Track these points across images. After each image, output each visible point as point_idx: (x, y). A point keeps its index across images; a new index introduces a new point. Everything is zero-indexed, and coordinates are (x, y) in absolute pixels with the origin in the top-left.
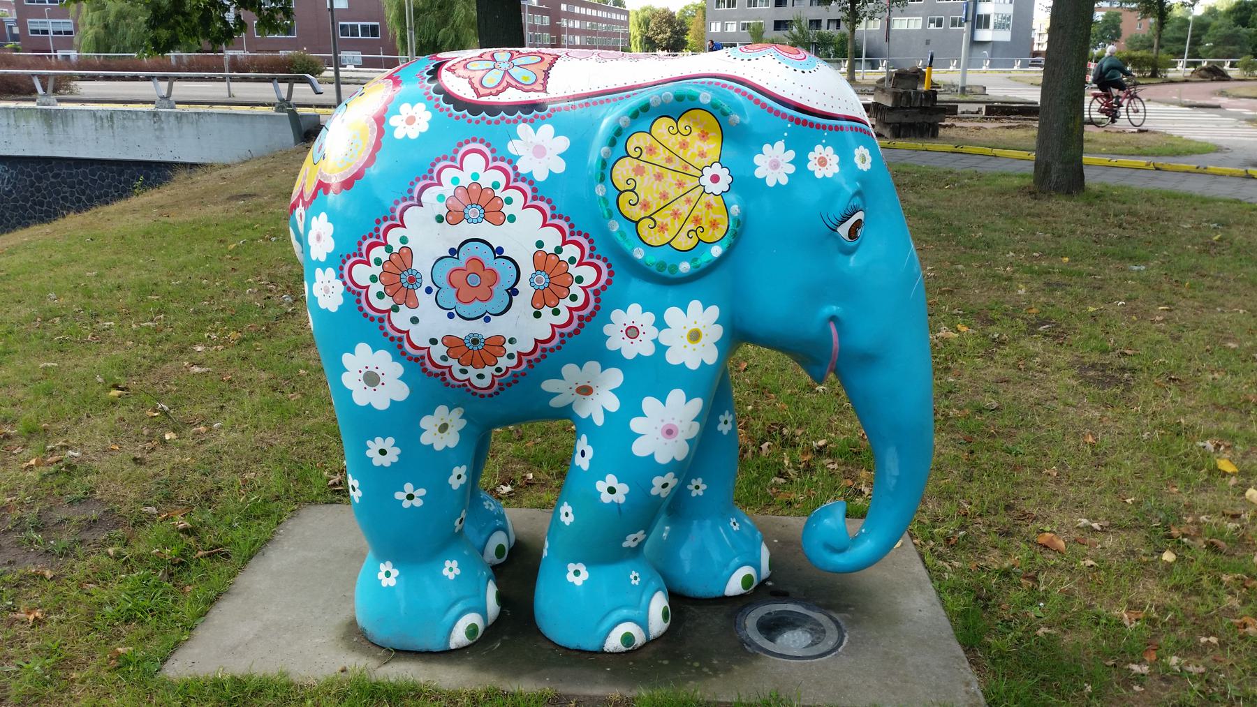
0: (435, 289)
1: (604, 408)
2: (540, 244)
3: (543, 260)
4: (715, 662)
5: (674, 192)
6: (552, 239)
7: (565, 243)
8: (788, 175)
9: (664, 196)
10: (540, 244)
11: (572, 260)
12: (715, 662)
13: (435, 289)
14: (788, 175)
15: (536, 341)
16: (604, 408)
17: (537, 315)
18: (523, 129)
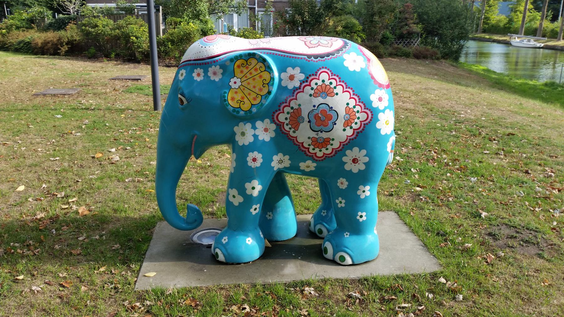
0: (316, 108)
1: (364, 156)
2: (348, 104)
3: (348, 110)
4: (436, 39)
5: (250, 81)
6: (352, 103)
7: (289, 106)
8: (346, 156)
9: (254, 79)
10: (348, 104)
11: (358, 112)
12: (436, 39)
13: (316, 108)
14: (346, 156)
15: (347, 136)
16: (364, 156)
17: (309, 138)
18: (345, 56)
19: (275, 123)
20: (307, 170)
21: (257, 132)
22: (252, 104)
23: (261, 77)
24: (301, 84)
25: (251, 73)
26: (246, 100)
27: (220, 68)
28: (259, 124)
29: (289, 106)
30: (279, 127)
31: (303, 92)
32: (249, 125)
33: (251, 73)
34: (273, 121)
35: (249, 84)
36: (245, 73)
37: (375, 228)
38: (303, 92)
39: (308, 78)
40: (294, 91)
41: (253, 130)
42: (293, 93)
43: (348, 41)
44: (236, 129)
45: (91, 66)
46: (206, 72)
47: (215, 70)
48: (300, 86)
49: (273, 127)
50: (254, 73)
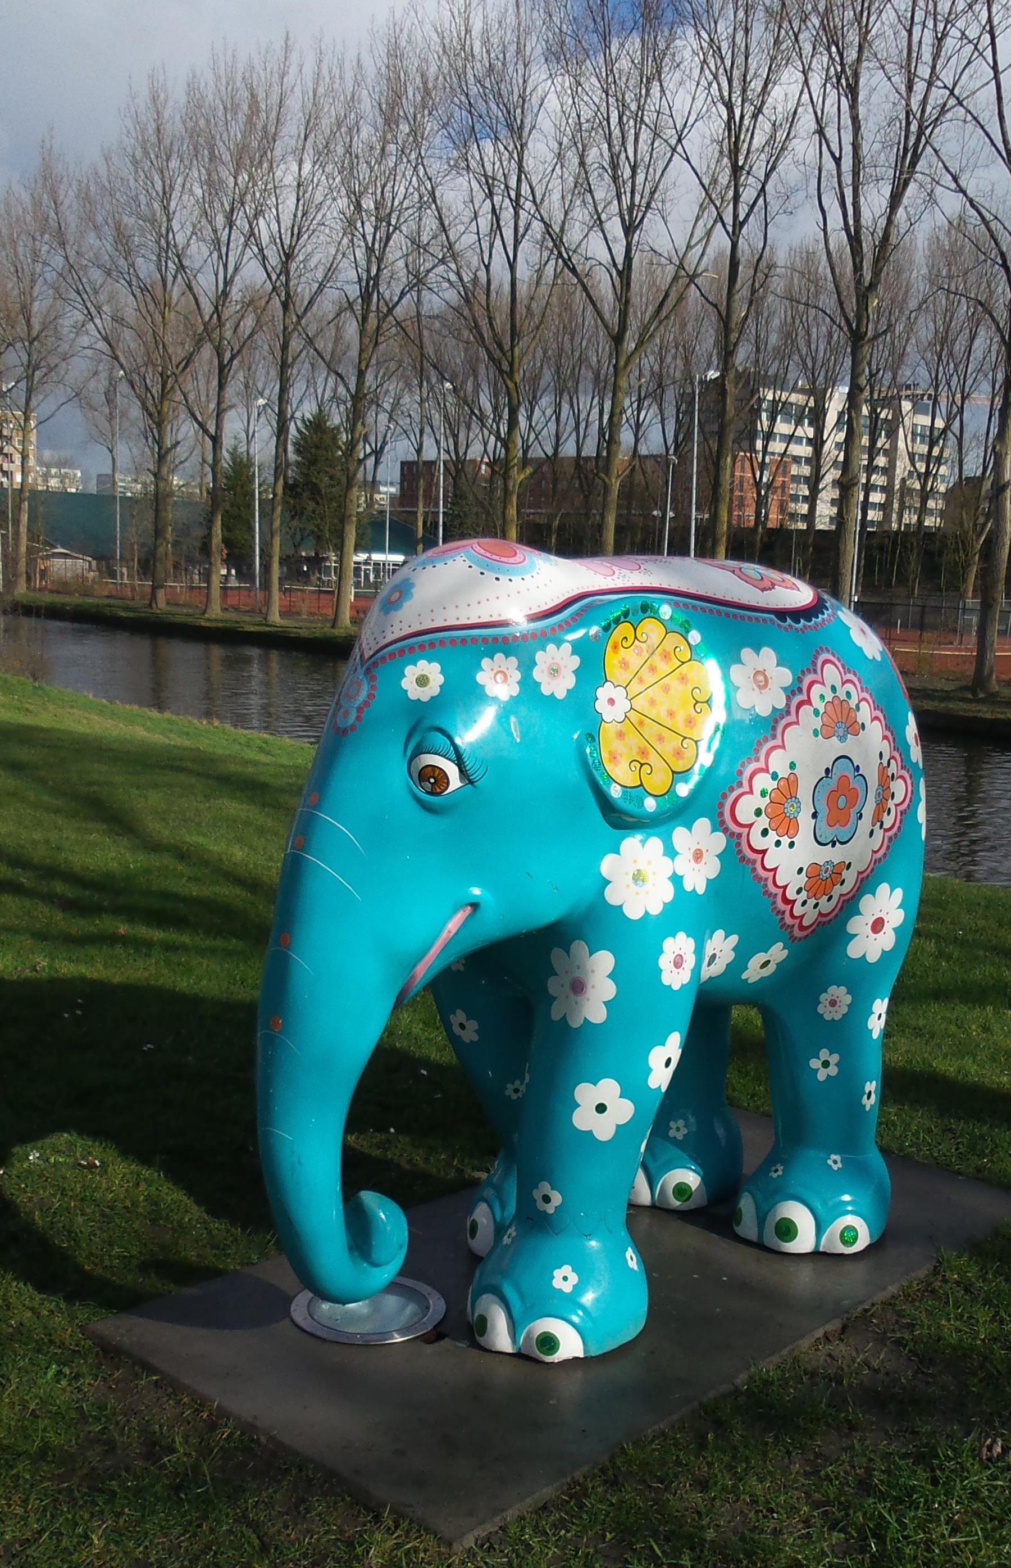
19: (725, 831)
20: (457, 1030)
21: (666, 867)
22: (673, 772)
23: (683, 679)
24: (788, 699)
25: (653, 669)
26: (653, 758)
27: (573, 654)
28: (680, 835)
29: (767, 771)
30: (735, 840)
31: (797, 723)
32: (655, 844)
33: (653, 669)
34: (720, 825)
35: (652, 702)
36: (634, 666)
37: (723, 1141)
38: (797, 723)
39: (800, 680)
40: (776, 721)
41: (667, 859)
42: (774, 728)
43: (826, 597)
44: (607, 865)
45: (815, 460)
46: (527, 666)
47: (558, 660)
48: (788, 705)
49: (719, 841)
50: (664, 668)
